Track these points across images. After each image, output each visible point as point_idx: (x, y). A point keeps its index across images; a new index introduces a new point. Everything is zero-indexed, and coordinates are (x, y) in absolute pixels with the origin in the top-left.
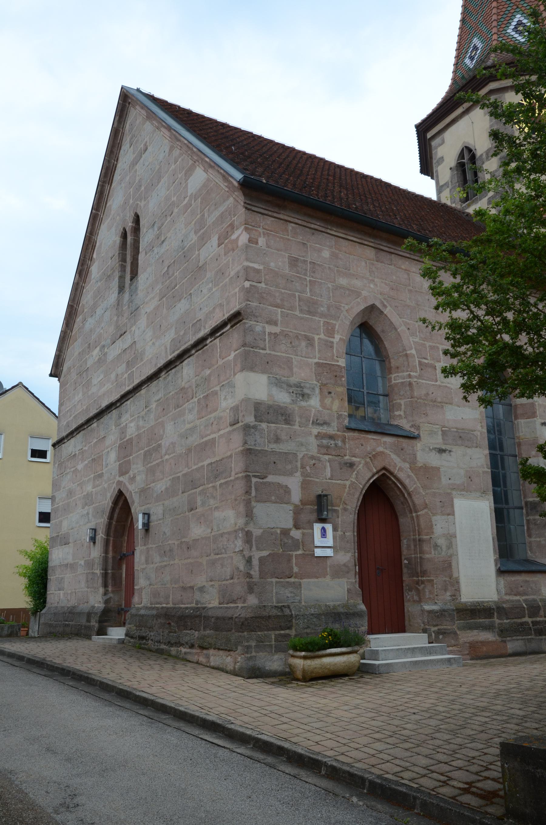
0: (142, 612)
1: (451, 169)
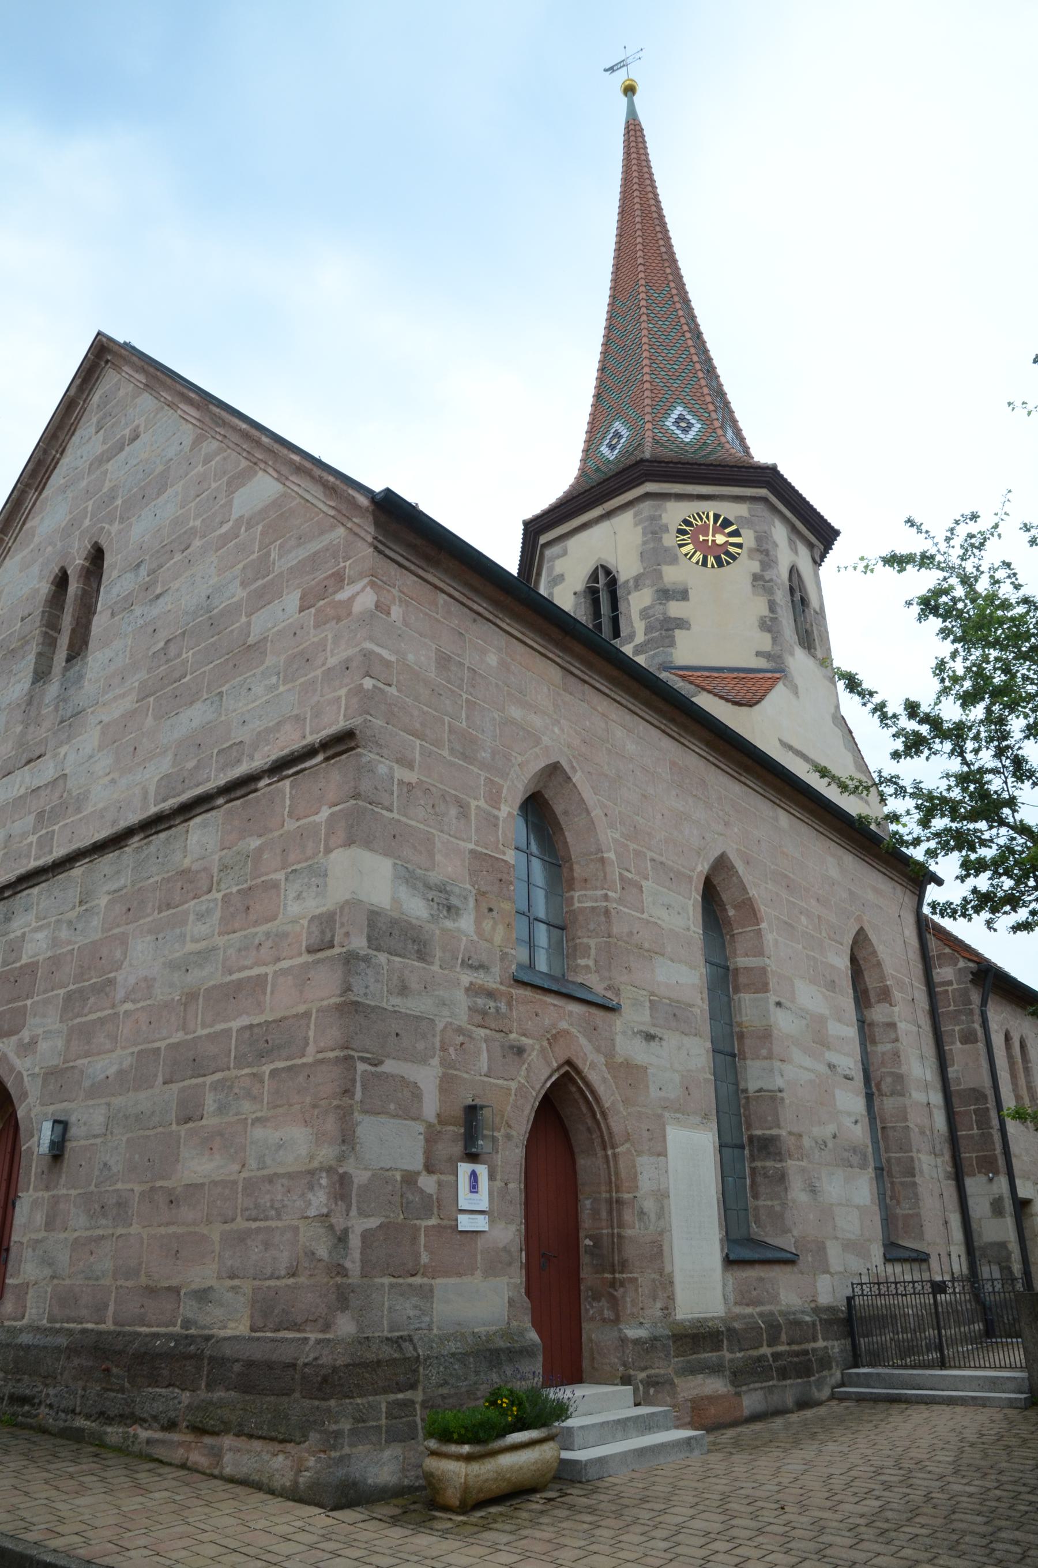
0: (25, 1339)
1: (575, 594)
